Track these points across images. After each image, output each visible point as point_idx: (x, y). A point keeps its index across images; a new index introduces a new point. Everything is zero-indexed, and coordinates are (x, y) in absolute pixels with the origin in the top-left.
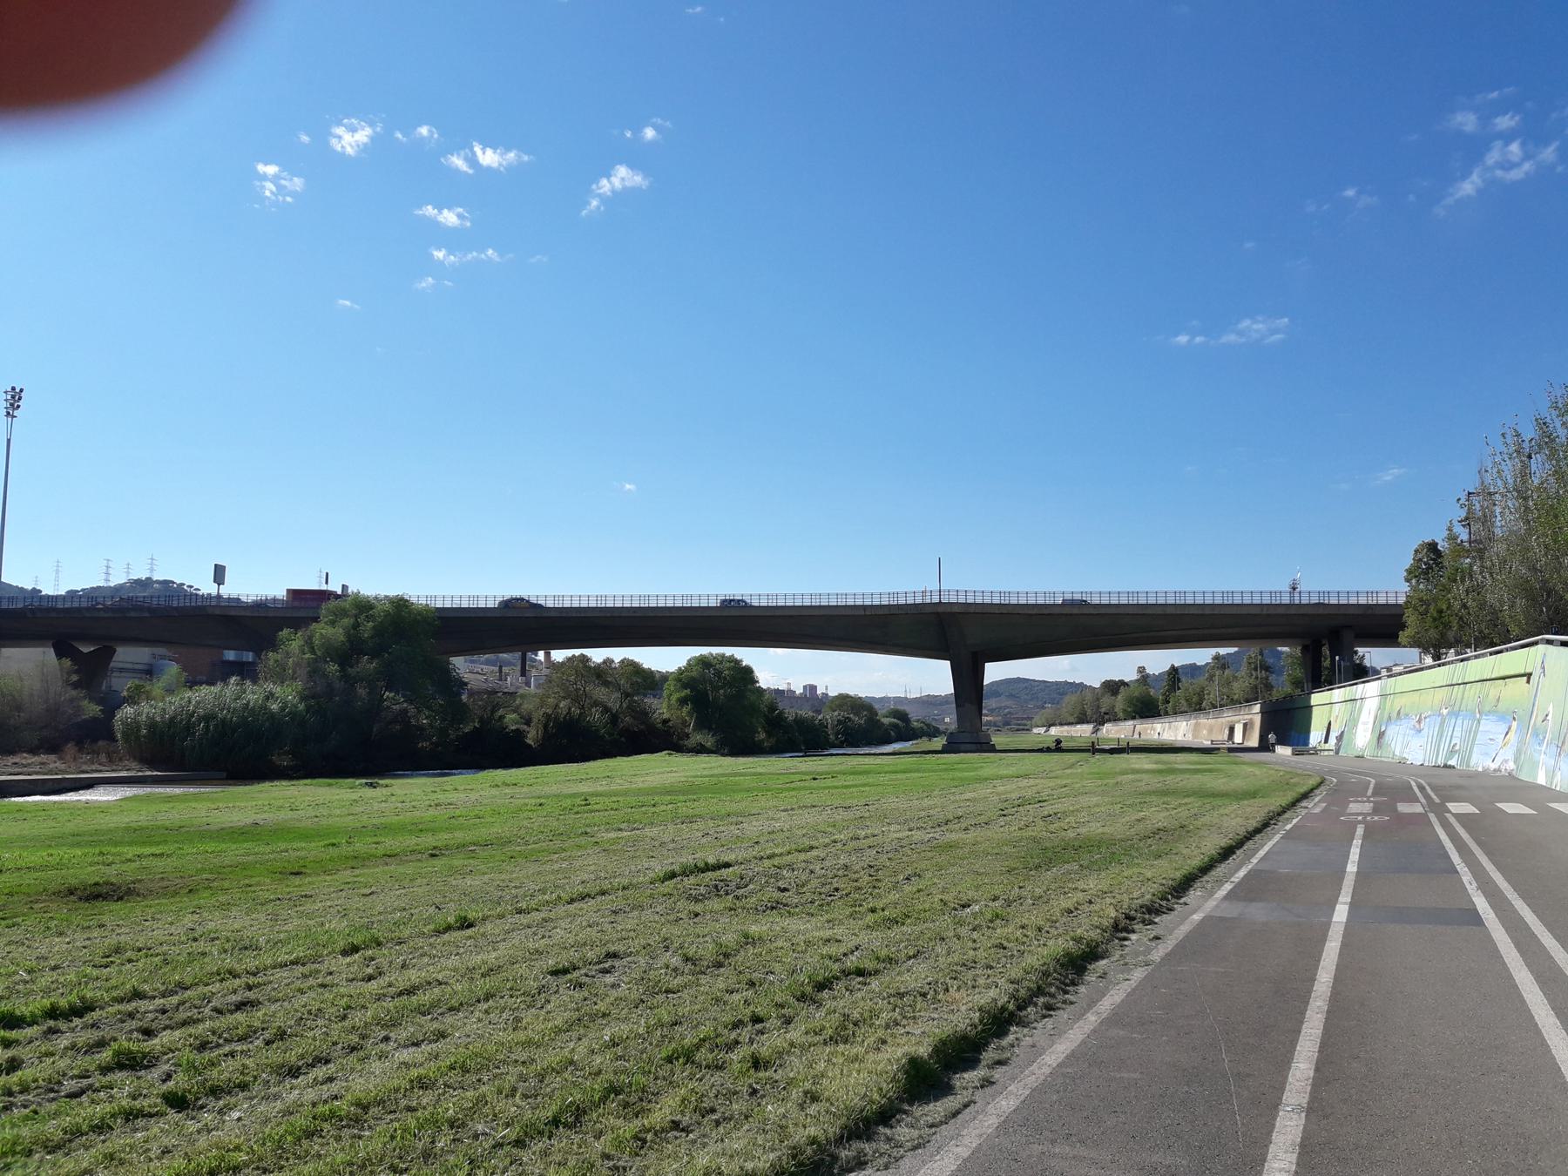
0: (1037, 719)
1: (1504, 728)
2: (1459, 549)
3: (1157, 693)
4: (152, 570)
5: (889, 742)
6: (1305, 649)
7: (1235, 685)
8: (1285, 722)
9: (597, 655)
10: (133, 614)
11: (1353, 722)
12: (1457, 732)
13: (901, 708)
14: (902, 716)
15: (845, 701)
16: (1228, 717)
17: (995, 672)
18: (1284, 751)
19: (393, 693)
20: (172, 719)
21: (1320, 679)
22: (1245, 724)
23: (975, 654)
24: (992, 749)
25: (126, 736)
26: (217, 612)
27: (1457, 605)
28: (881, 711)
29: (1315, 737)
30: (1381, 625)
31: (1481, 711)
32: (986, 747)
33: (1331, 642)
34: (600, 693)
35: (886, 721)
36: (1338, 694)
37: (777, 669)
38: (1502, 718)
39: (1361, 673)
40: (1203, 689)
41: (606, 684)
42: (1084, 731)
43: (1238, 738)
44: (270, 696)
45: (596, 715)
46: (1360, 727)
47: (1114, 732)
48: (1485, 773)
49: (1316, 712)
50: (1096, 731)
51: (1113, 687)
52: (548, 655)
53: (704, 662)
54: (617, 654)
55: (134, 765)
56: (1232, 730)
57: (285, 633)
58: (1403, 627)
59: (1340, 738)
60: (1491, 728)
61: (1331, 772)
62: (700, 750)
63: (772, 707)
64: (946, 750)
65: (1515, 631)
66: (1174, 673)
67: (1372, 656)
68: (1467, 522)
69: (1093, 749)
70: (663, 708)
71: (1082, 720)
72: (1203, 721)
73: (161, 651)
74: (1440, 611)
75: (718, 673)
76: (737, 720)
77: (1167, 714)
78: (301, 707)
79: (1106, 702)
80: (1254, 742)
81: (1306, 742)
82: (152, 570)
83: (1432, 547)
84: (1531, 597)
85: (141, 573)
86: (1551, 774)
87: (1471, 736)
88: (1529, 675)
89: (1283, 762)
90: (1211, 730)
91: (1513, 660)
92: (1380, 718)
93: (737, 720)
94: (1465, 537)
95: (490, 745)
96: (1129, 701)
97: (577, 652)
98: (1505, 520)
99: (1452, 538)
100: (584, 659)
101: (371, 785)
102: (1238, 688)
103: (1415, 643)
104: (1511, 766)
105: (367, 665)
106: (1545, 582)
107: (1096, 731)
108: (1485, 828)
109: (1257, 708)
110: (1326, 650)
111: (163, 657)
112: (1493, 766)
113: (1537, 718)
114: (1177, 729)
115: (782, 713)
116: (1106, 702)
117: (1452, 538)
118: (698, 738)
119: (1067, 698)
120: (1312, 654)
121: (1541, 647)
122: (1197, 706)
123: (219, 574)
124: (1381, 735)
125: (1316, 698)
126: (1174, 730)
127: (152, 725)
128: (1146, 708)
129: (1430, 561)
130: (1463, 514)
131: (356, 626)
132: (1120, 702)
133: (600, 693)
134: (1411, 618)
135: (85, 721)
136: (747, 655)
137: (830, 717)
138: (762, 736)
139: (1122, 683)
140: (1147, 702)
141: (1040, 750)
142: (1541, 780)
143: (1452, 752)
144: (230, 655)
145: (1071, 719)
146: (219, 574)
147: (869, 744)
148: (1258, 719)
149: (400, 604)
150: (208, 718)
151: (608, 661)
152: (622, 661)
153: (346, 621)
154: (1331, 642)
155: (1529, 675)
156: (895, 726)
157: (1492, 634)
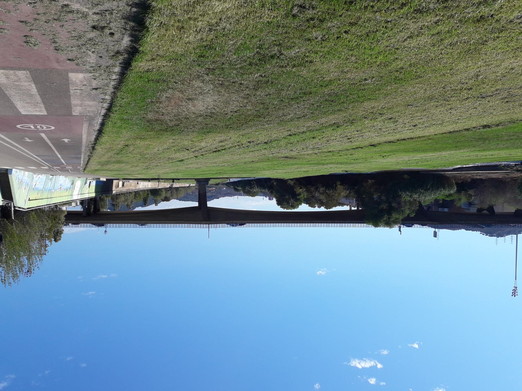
0: (194, 189)
1: (37, 186)
2: (49, 238)
3: (151, 197)
4: (497, 240)
5: (239, 181)
6: (99, 210)
7: (123, 199)
8: (104, 188)
9: (323, 209)
10: (463, 222)
11: (81, 188)
12: (50, 185)
13: (236, 192)
14: (236, 190)
15: (253, 195)
16: (124, 189)
17: (196, 204)
18: (103, 179)
19: (382, 198)
20: (438, 189)
21: (91, 201)
22: (118, 187)
23: (200, 209)
24: (196, 179)
25: (453, 184)
26: (435, 223)
27: (50, 222)
28: (242, 192)
29: (94, 183)
30: (74, 218)
31: (43, 190)
32: (198, 180)
33: (92, 212)
34: (322, 197)
35: (240, 188)
36: (86, 196)
37: (266, 204)
38: (37, 189)
39: (82, 202)
40: (135, 198)
41: (320, 200)
42: (176, 185)
43: (121, 183)
44: (411, 196)
45: (322, 189)
46: (79, 186)
47: (167, 185)
48: (42, 174)
49: (94, 191)
50: (172, 185)
51: (167, 199)
52: (350, 208)
53: (293, 207)
54: (316, 209)
55: (448, 175)
56: (123, 185)
57: (413, 215)
58: (65, 216)
59: (86, 183)
60: (40, 186)
61: (82, 174)
62: (291, 180)
63: (271, 192)
64: (209, 179)
65: (33, 213)
66: (145, 204)
67: (79, 208)
68: (46, 246)
69: (173, 180)
70: (301, 191)
71: (177, 189)
72: (134, 188)
73: (466, 211)
74: (54, 220)
75: (288, 203)
76: (283, 190)
77: (148, 190)
78: (400, 193)
79: (169, 194)
80: (115, 182)
81: (97, 182)
82: (497, 240)
83: (56, 240)
84: (28, 223)
85: (501, 239)
86: (24, 174)
87: (46, 183)
88: (29, 200)
89: (103, 176)
90: (131, 185)
91: (34, 204)
92: (76, 189)
93: (283, 190)
94: (47, 241)
95: (352, 182)
96: (160, 195)
97: (329, 210)
98: (35, 245)
99: (51, 241)
100: (326, 208)
101: (346, 171)
102: (122, 198)
103: (63, 211)
104: (35, 176)
105: (384, 206)
106: (24, 227)
107: (172, 185)
108: (38, 165)
109: (114, 192)
110: (92, 210)
111: (466, 209)
112: (40, 176)
113: (27, 188)
114: (143, 186)
115: (268, 191)
116: (169, 194)
117: (51, 241)
118: (292, 183)
119: (183, 196)
120: (97, 210)
121: (26, 207)
122: (137, 193)
123: (435, 235)
124: (72, 184)
125: (93, 195)
126: (143, 185)
127: (444, 188)
128: (155, 192)
129: (57, 235)
130: (47, 249)
131: (389, 218)
132: (164, 194)
133: (322, 197)
134: (63, 218)
135: (473, 189)
136: (279, 209)
137: (256, 190)
138: (275, 183)
139: (163, 201)
140: (155, 194)
141: (179, 179)
142: (27, 173)
143: (51, 179)
144: (446, 210)
145: (181, 189)
146: (435, 235)
147: (245, 181)
148: (114, 188)
149: (376, 225)
150: (427, 190)
151: (319, 207)
152: (315, 207)
153: (392, 219)
154: (92, 212)
155: (29, 200)
156: (238, 187)
157: (38, 211)
